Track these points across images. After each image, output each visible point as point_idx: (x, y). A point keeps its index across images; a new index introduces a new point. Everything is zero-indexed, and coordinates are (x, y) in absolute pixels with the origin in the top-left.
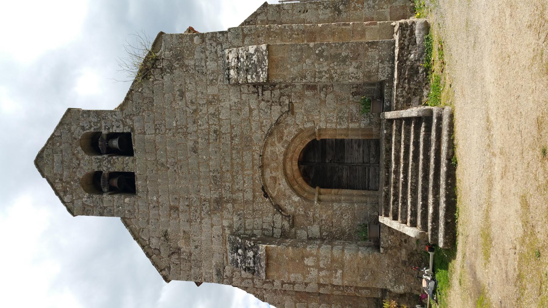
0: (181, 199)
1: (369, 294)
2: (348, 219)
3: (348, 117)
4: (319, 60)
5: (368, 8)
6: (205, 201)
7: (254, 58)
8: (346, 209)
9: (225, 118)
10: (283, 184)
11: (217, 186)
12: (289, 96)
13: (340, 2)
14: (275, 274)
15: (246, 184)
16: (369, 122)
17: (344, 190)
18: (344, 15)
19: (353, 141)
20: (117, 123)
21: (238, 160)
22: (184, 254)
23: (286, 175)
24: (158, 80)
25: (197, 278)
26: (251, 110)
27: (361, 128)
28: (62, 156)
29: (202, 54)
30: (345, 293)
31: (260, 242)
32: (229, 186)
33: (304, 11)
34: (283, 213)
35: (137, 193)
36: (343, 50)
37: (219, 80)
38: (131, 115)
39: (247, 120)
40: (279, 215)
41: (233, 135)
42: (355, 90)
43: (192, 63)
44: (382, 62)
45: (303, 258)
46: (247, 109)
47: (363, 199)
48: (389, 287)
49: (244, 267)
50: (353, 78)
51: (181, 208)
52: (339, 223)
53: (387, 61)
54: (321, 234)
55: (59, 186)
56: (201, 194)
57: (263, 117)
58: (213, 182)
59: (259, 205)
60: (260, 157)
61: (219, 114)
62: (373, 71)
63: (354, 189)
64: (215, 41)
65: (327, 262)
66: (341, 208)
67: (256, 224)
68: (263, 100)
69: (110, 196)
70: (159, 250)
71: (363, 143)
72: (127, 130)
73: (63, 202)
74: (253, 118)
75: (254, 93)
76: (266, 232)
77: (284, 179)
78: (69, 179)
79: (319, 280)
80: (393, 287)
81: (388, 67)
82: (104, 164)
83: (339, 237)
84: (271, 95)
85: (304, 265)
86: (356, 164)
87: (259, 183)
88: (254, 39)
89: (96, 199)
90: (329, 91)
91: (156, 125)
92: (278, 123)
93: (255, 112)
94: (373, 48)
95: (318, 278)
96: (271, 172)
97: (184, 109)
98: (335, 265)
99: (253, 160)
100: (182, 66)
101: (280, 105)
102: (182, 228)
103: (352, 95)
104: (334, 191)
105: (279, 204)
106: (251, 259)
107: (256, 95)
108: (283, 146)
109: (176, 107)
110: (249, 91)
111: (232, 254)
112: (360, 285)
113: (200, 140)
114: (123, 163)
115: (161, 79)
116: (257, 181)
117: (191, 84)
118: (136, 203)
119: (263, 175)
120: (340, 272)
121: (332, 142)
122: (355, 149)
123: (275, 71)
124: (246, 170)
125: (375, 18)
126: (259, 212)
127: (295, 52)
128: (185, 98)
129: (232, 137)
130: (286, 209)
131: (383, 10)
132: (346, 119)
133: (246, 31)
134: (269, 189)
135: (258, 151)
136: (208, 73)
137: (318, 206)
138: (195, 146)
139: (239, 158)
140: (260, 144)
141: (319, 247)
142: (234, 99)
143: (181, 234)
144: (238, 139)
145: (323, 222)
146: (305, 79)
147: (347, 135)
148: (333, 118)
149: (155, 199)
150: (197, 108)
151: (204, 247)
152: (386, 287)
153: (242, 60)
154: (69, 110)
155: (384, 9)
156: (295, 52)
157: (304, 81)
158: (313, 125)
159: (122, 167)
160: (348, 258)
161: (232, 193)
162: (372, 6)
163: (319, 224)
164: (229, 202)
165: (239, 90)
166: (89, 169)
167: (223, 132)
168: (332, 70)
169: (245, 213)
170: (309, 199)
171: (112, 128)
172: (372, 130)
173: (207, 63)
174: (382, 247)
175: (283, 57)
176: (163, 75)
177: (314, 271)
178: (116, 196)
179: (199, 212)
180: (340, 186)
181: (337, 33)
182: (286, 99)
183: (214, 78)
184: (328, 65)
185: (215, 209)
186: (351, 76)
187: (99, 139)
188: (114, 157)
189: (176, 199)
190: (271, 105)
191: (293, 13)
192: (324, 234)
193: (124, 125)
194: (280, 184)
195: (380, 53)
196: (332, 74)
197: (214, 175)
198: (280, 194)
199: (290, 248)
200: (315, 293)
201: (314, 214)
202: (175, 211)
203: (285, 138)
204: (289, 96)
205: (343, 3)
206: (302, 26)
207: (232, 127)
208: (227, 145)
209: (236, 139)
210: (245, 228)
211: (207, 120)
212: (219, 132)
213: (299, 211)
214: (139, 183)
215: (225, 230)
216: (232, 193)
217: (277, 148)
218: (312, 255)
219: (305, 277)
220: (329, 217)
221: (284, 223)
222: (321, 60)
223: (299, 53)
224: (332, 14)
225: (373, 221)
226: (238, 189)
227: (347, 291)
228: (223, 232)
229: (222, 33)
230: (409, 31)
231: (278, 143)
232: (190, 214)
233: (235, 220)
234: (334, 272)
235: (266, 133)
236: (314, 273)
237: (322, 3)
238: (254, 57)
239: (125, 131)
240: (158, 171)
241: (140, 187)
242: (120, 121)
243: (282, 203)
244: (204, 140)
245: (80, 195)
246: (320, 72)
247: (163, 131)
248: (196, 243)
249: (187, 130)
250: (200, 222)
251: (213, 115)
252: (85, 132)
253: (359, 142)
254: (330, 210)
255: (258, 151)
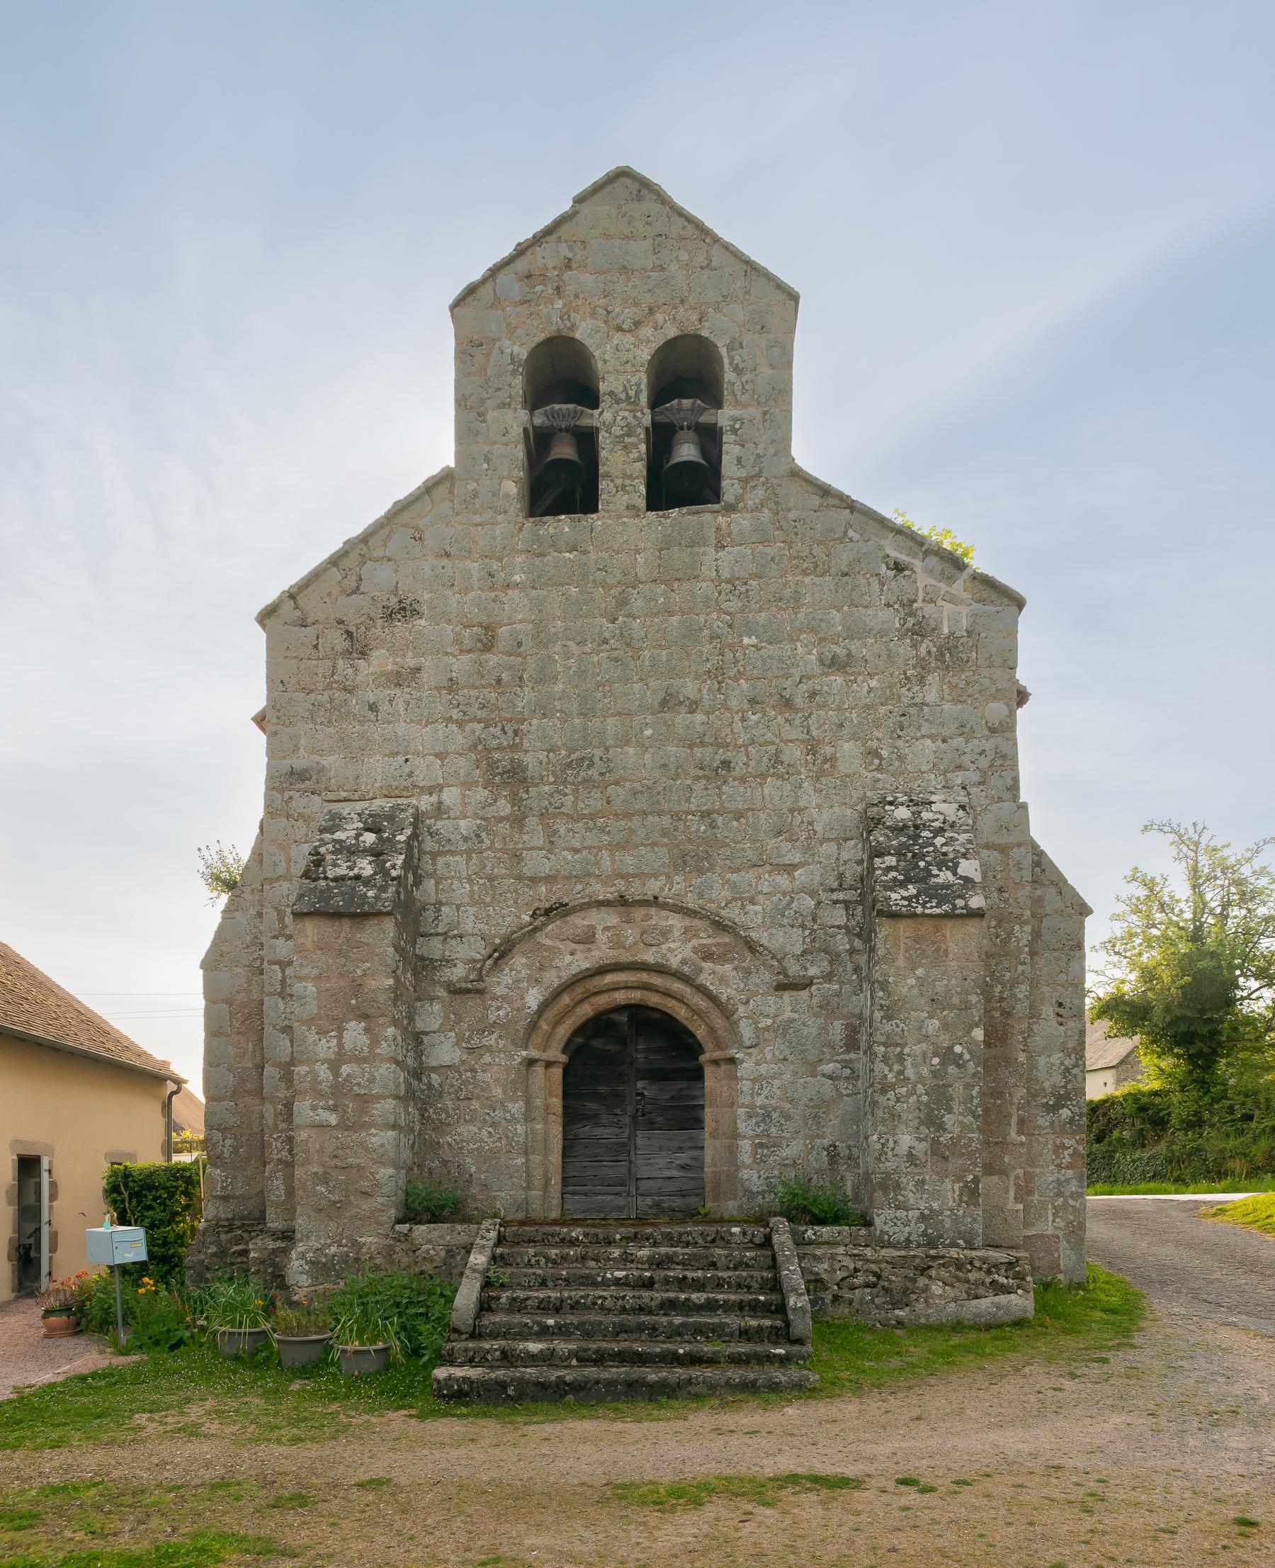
0: (520, 659)
1: (274, 1198)
2: (482, 1140)
3: (768, 1136)
4: (936, 1054)
5: (1058, 1181)
6: (516, 733)
7: (945, 876)
8: (510, 1135)
9: (766, 791)
10: (575, 962)
11: (563, 772)
12: (828, 977)
13: (1077, 1111)
14: (310, 939)
15: (569, 857)
16: (755, 1190)
17: (561, 1129)
18: (1043, 1121)
19: (695, 1153)
20: (752, 458)
21: (641, 832)
22: (350, 671)
23: (602, 971)
24: (882, 590)
25: (279, 711)
26: (789, 869)
27: (737, 1170)
28: (645, 269)
29: (956, 725)
30: (271, 1136)
31: (402, 897)
32: (563, 805)
33: (1061, 1016)
34: (490, 962)
35: (531, 519)
36: (960, 1118)
37: (879, 776)
38: (777, 503)
39: (762, 860)
40: (484, 952)
41: (715, 816)
42: (844, 1152)
43: (931, 695)
44: (923, 1218)
45: (365, 1016)
46: (798, 858)
47: (538, 1181)
48: (301, 1247)
49: (322, 850)
50: (883, 1145)
51: (492, 659)
52: (468, 1117)
53: (926, 1229)
54: (435, 1069)
55: (546, 257)
56: (535, 721)
57: (768, 903)
58: (573, 757)
59: (509, 895)
60: (652, 898)
61: (781, 777)
62: (899, 1197)
63: (564, 1156)
64: (992, 766)
65: (359, 1084)
66: (513, 1120)
67: (454, 887)
68: (819, 903)
69: (521, 430)
70: (356, 591)
71: (692, 1178)
72: (729, 488)
73: (495, 271)
74: (767, 876)
75: (841, 877)
76: (429, 914)
77: (588, 966)
78: (569, 290)
79: (301, 1063)
80: (302, 1256)
81: (910, 1233)
82: (622, 413)
83: (429, 1117)
84: (833, 927)
85: (342, 1022)
86: (633, 1159)
87: (574, 893)
88: (994, 877)
89: (510, 386)
90: (842, 1085)
91: (746, 584)
92: (751, 946)
93: (783, 881)
94: (960, 1195)
95: (309, 1060)
96: (607, 929)
97: (793, 671)
98: (351, 1105)
99: (642, 876)
100: (922, 664)
101: (804, 953)
102: (426, 662)
103: (830, 1146)
104: (557, 1103)
105: (515, 950)
106: (351, 868)
107: (835, 885)
108: (684, 962)
109: (799, 644)
110: (845, 862)
111: (359, 815)
112: (298, 1172)
113: (699, 717)
114: (625, 476)
115: (883, 602)
116: (579, 887)
117: (869, 692)
118: (500, 518)
119: (600, 904)
120: (333, 1119)
121: (695, 1098)
122: (677, 1159)
123: (907, 934)
124: (612, 855)
125: (1031, 1198)
126: (488, 893)
127: (958, 989)
128: (827, 674)
129: (709, 814)
130: (502, 971)
131: (1050, 1218)
132: (762, 1131)
133: (1016, 853)
134: (558, 923)
135: (670, 890)
136: (900, 743)
137: (515, 1060)
138: (681, 703)
139: (647, 834)
140: (690, 895)
141: (397, 1063)
142: (822, 820)
143: (411, 661)
144: (705, 832)
145: (469, 1074)
146: (883, 1017)
147: (714, 1135)
148: (767, 1098)
149: (517, 578)
150: (798, 711)
151: (377, 731)
152: (301, 1241)
153: (939, 841)
154: (794, 297)
155: (1054, 1221)
156: (958, 989)
157: (878, 1015)
158: (748, 1043)
159: (614, 473)
160: (374, 1140)
161: (542, 814)
162: (1063, 1190)
163: (463, 1062)
164: (513, 806)
165: (849, 835)
166: (605, 361)
167: (725, 788)
168: (905, 1089)
169: (485, 855)
170: (533, 1036)
171: (735, 443)
172: (730, 1199)
173: (928, 742)
174: (410, 1230)
175: (947, 956)
176: (896, 606)
177: (329, 1048)
178: (520, 453)
179: (480, 714)
180: (571, 1117)
181: (999, 1102)
182: (822, 969)
183: (884, 762)
184: (921, 1080)
185: (492, 765)
186: (888, 1140)
187: (699, 402)
188: (643, 447)
189: (520, 644)
190: (803, 927)
191: (1058, 985)
192: (434, 1076)
193: (744, 481)
194: (572, 954)
195: (948, 1213)
196: (894, 1090)
197: (596, 760)
198: (545, 954)
199: (391, 982)
200: (263, 1056)
201: (489, 1049)
202: (480, 640)
203: (707, 965)
204: (828, 977)
205: (1077, 1118)
206: (1021, 1009)
207: (738, 815)
208: (688, 800)
209: (703, 828)
210: (440, 853)
211: (762, 740)
212: (724, 776)
213: (498, 1009)
214: (563, 525)
215: (431, 794)
216: (542, 814)
217: (678, 944)
218: (375, 1042)
219: (309, 1022)
220: (483, 1090)
221: (460, 965)
222: (936, 1061)
223: (956, 1000)
224: (1049, 1090)
225: (480, 1205)
226: (555, 832)
227: (276, 1140)
228: (422, 788)
229: (1014, 787)
230: (1005, 1281)
231: (694, 947)
232: (474, 687)
233: (462, 823)
234: (331, 1102)
235: (723, 913)
236: (325, 1047)
237: (1080, 1062)
238: (949, 873)
239: (725, 484)
240: (603, 587)
241: (551, 530)
242: (757, 469)
243: (518, 960)
244: (699, 729)
245: (520, 331)
246: (901, 1058)
247: (724, 606)
248: (384, 708)
249: (730, 678)
250: (449, 720)
251: (777, 759)
252: (723, 351)
253: (694, 1167)
254: (504, 1092)
255: (670, 890)
